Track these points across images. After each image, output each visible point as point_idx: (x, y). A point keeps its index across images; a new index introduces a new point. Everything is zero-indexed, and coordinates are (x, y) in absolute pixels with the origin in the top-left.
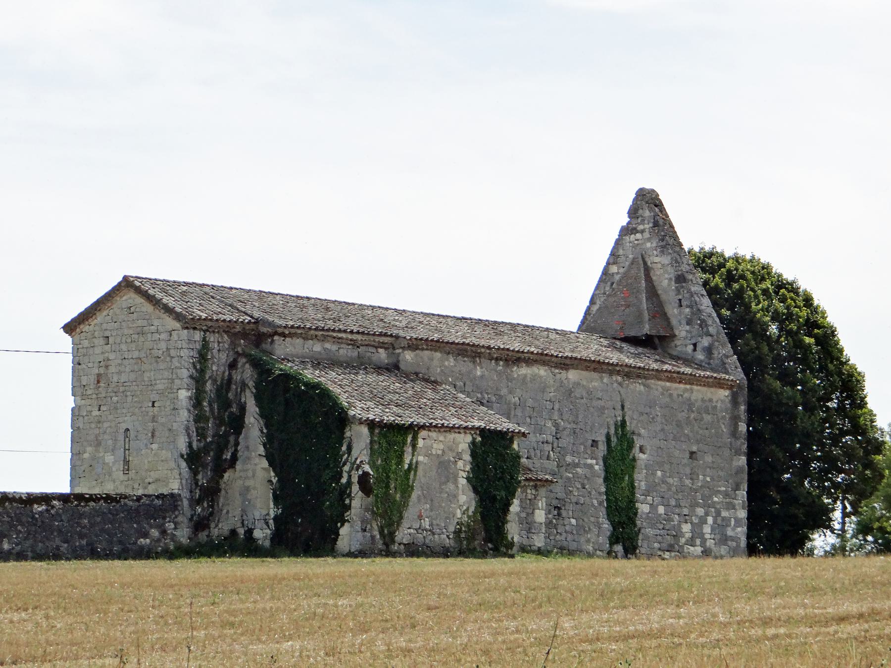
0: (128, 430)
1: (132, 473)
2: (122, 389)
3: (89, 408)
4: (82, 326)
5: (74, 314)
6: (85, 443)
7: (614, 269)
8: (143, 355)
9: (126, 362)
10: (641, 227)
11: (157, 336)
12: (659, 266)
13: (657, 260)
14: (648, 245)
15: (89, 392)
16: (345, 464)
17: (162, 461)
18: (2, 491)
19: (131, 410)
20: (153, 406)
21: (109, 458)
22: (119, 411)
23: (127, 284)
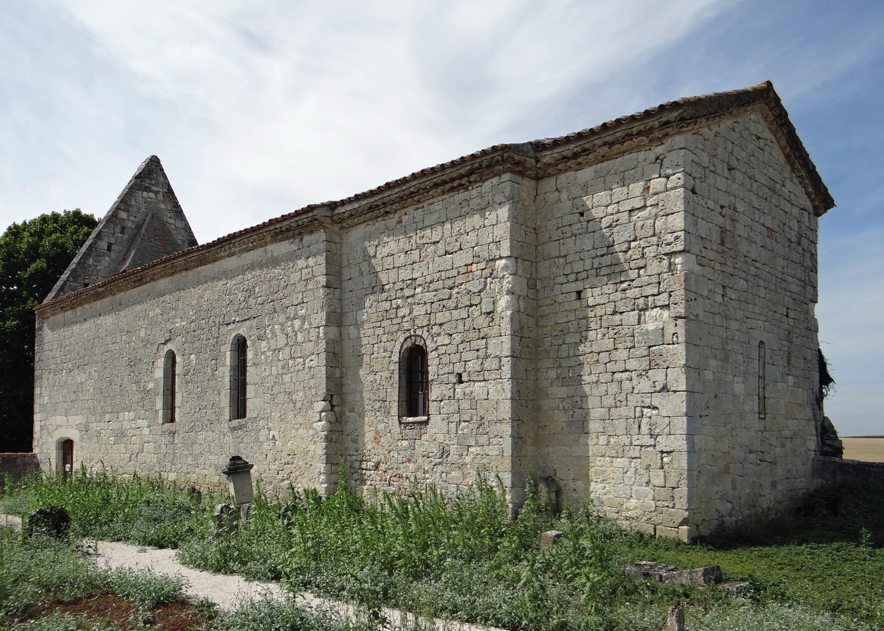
7: (123, 215)
10: (154, 188)
13: (171, 221)
14: (163, 206)
21: (739, 388)
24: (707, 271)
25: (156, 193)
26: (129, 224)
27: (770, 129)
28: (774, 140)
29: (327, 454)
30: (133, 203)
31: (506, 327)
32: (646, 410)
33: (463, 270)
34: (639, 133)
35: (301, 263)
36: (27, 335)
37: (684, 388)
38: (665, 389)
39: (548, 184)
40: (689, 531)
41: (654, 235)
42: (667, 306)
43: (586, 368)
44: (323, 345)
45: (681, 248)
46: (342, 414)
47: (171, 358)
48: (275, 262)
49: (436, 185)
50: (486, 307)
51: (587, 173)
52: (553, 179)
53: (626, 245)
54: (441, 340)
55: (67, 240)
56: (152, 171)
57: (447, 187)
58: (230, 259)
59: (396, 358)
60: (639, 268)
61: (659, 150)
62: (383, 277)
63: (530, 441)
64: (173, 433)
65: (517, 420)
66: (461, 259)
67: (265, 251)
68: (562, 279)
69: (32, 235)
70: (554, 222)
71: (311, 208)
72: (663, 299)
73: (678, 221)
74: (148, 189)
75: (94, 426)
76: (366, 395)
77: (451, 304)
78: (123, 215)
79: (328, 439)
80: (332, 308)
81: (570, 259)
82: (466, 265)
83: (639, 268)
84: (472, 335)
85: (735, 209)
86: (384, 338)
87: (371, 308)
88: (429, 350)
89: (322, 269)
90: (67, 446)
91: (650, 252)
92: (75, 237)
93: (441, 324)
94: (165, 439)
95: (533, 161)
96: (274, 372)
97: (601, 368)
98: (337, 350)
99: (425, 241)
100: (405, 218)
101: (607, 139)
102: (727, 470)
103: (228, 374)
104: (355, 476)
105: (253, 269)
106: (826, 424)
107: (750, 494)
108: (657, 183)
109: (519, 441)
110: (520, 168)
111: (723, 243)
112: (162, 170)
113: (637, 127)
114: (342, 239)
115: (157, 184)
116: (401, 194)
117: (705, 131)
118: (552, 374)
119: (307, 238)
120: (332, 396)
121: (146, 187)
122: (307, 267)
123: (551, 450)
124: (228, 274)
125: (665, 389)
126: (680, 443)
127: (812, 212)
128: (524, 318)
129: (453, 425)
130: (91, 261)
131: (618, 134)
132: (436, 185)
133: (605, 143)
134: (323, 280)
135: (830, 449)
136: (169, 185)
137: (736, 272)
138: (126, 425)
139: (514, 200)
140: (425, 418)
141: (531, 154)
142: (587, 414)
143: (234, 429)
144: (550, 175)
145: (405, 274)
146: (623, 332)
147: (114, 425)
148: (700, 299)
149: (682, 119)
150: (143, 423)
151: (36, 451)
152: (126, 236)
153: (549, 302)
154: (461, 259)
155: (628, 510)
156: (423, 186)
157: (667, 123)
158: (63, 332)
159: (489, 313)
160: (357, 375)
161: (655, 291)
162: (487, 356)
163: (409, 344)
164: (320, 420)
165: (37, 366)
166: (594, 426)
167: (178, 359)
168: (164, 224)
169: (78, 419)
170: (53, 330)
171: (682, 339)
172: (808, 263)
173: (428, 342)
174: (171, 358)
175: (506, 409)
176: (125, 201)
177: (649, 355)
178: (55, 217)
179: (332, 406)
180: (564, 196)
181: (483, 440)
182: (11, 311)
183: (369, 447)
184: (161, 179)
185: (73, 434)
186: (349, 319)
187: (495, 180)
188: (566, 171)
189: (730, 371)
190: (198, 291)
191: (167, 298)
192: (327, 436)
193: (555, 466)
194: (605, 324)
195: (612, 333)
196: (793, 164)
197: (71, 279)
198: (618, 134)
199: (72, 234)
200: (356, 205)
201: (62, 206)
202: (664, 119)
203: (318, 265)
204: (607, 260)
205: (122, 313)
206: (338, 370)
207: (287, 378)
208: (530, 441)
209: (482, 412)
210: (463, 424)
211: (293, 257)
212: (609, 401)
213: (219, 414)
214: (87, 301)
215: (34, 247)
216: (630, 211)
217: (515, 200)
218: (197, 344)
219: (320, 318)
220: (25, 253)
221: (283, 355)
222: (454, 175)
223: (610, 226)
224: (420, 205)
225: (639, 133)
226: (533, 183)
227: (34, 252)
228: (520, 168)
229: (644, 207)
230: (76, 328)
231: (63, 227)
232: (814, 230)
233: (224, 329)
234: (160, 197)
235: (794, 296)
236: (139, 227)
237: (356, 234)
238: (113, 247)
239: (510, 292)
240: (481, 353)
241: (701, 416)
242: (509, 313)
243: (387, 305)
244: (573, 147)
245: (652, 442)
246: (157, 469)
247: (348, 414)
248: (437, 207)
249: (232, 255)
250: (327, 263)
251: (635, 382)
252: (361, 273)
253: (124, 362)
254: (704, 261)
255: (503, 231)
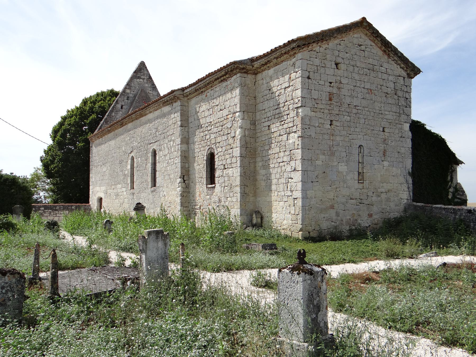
0: (360, 146)
1: (366, 183)
2: (354, 111)
3: (321, 121)
4: (315, 45)
5: (310, 32)
6: (318, 152)
7: (128, 91)
8: (373, 87)
9: (357, 89)
10: (142, 77)
11: (385, 76)
12: (152, 95)
13: (151, 92)
14: (147, 85)
15: (320, 106)
16: (450, 187)
17: (394, 176)
18: (6, 171)
19: (364, 130)
20: (383, 131)
21: (343, 168)
22: (352, 129)
23: (363, 25)
24: (319, 115)
25: (143, 79)
26: (131, 95)
27: (370, 39)
28: (373, 44)
29: (181, 203)
30: (133, 85)
31: (238, 143)
32: (290, 180)
33: (225, 118)
34: (285, 53)
35: (173, 116)
36: (87, 151)
37: (300, 169)
38: (295, 170)
39: (259, 76)
40: (302, 234)
41: (292, 99)
42: (295, 132)
43: (271, 162)
44: (180, 153)
45: (300, 105)
46: (189, 184)
47: (133, 159)
48: (164, 115)
49: (216, 80)
50: (233, 135)
51: (271, 71)
52: (261, 74)
53: (283, 104)
54: (220, 150)
55: (105, 104)
56: (142, 68)
57: (220, 80)
58: (150, 114)
59: (205, 158)
60: (288, 115)
61: (294, 60)
62: (202, 121)
63: (251, 195)
64: (133, 194)
65: (243, 185)
66: (225, 112)
67: (161, 111)
68: (263, 120)
69: (91, 103)
70: (261, 94)
71: (173, 92)
72: (294, 129)
73: (299, 93)
74: (139, 78)
75: (109, 191)
76: (197, 175)
77: (222, 133)
78: (128, 91)
79: (182, 196)
80: (184, 136)
81: (266, 111)
82: (227, 116)
83: (288, 115)
84: (228, 147)
85: (341, 83)
86: (202, 149)
87: (199, 135)
88: (215, 154)
89: (179, 119)
90: (100, 200)
91: (291, 107)
92: (109, 102)
93: (219, 142)
94: (131, 197)
95: (251, 67)
96: (165, 166)
97: (275, 161)
98: (186, 155)
99: (214, 104)
100: (208, 94)
101: (274, 56)
102: (332, 207)
103: (150, 167)
104: (193, 212)
105: (157, 118)
106: (458, 187)
107: (350, 219)
108: (293, 75)
109: (244, 195)
110: (244, 71)
111: (330, 99)
112: (146, 68)
113: (283, 51)
114: (188, 104)
115: (144, 75)
116: (204, 84)
117: (317, 49)
118: (260, 164)
119: (174, 104)
120: (184, 176)
121: (138, 77)
122: (174, 118)
123: (260, 199)
124: (150, 121)
125: (295, 170)
126: (298, 194)
127: (406, 76)
128: (248, 139)
129: (222, 188)
130: (113, 114)
131: (278, 54)
132: (216, 80)
133: (275, 58)
134: (179, 123)
135: (459, 201)
136: (150, 75)
137: (341, 113)
138: (119, 191)
139: (243, 86)
140: (214, 185)
141: (249, 63)
142: (271, 182)
143: (152, 192)
144: (260, 72)
145: (208, 121)
146: (282, 144)
147: (115, 191)
148: (311, 128)
149: (298, 46)
150: (124, 189)
151: (90, 203)
152: (129, 101)
153: (260, 131)
154: (225, 112)
155: (284, 225)
156: (211, 80)
157: (293, 48)
158: (99, 148)
159: (233, 137)
160: (194, 166)
161: (292, 125)
162: (233, 157)
163: (209, 152)
164: (179, 187)
165: (91, 164)
166: (274, 187)
167: (135, 160)
168: (146, 94)
169: (103, 188)
170: (96, 147)
171: (300, 147)
172: (402, 102)
173: (215, 151)
174: (133, 159)
175: (238, 181)
176: (129, 85)
177: (290, 155)
178: (102, 93)
179: (184, 181)
180: (264, 82)
181: (231, 194)
182: (81, 139)
183: (198, 199)
184: (146, 72)
185: (102, 195)
186: (191, 141)
187: (235, 77)
188: (265, 70)
189: (335, 160)
190: (140, 129)
191: (131, 132)
192: (181, 194)
193: (262, 206)
194: (277, 141)
195: (279, 144)
196: (389, 54)
197: (105, 123)
198: (278, 54)
199: (108, 101)
200: (190, 89)
201: (105, 88)
202: (291, 47)
203: (176, 117)
204: (277, 111)
205: (117, 139)
206: (187, 164)
207: (168, 168)
208: (251, 195)
209: (231, 182)
210: (226, 187)
211: (170, 113)
212: (278, 176)
213: (148, 185)
214: (105, 134)
215: (91, 108)
216: (285, 88)
217: (243, 85)
218: (140, 153)
219: (178, 141)
220: (88, 111)
221: (167, 158)
222: (221, 75)
223: (279, 95)
224: (212, 88)
225: (285, 53)
226: (253, 76)
227: (92, 111)
228: (244, 71)
229: (289, 86)
230: (103, 146)
231: (105, 98)
232: (409, 86)
233: (149, 146)
234: (145, 81)
235: (390, 121)
236: (135, 96)
237: (193, 101)
238: (124, 107)
239: (241, 127)
240: (231, 155)
241: (312, 182)
242: (239, 137)
243: (202, 134)
244: (263, 61)
245: (291, 194)
246: (128, 211)
247: (191, 184)
248: (217, 89)
249: (151, 112)
250: (181, 116)
251: (286, 167)
252: (195, 120)
253: (118, 162)
254: (315, 110)
255: (237, 100)
